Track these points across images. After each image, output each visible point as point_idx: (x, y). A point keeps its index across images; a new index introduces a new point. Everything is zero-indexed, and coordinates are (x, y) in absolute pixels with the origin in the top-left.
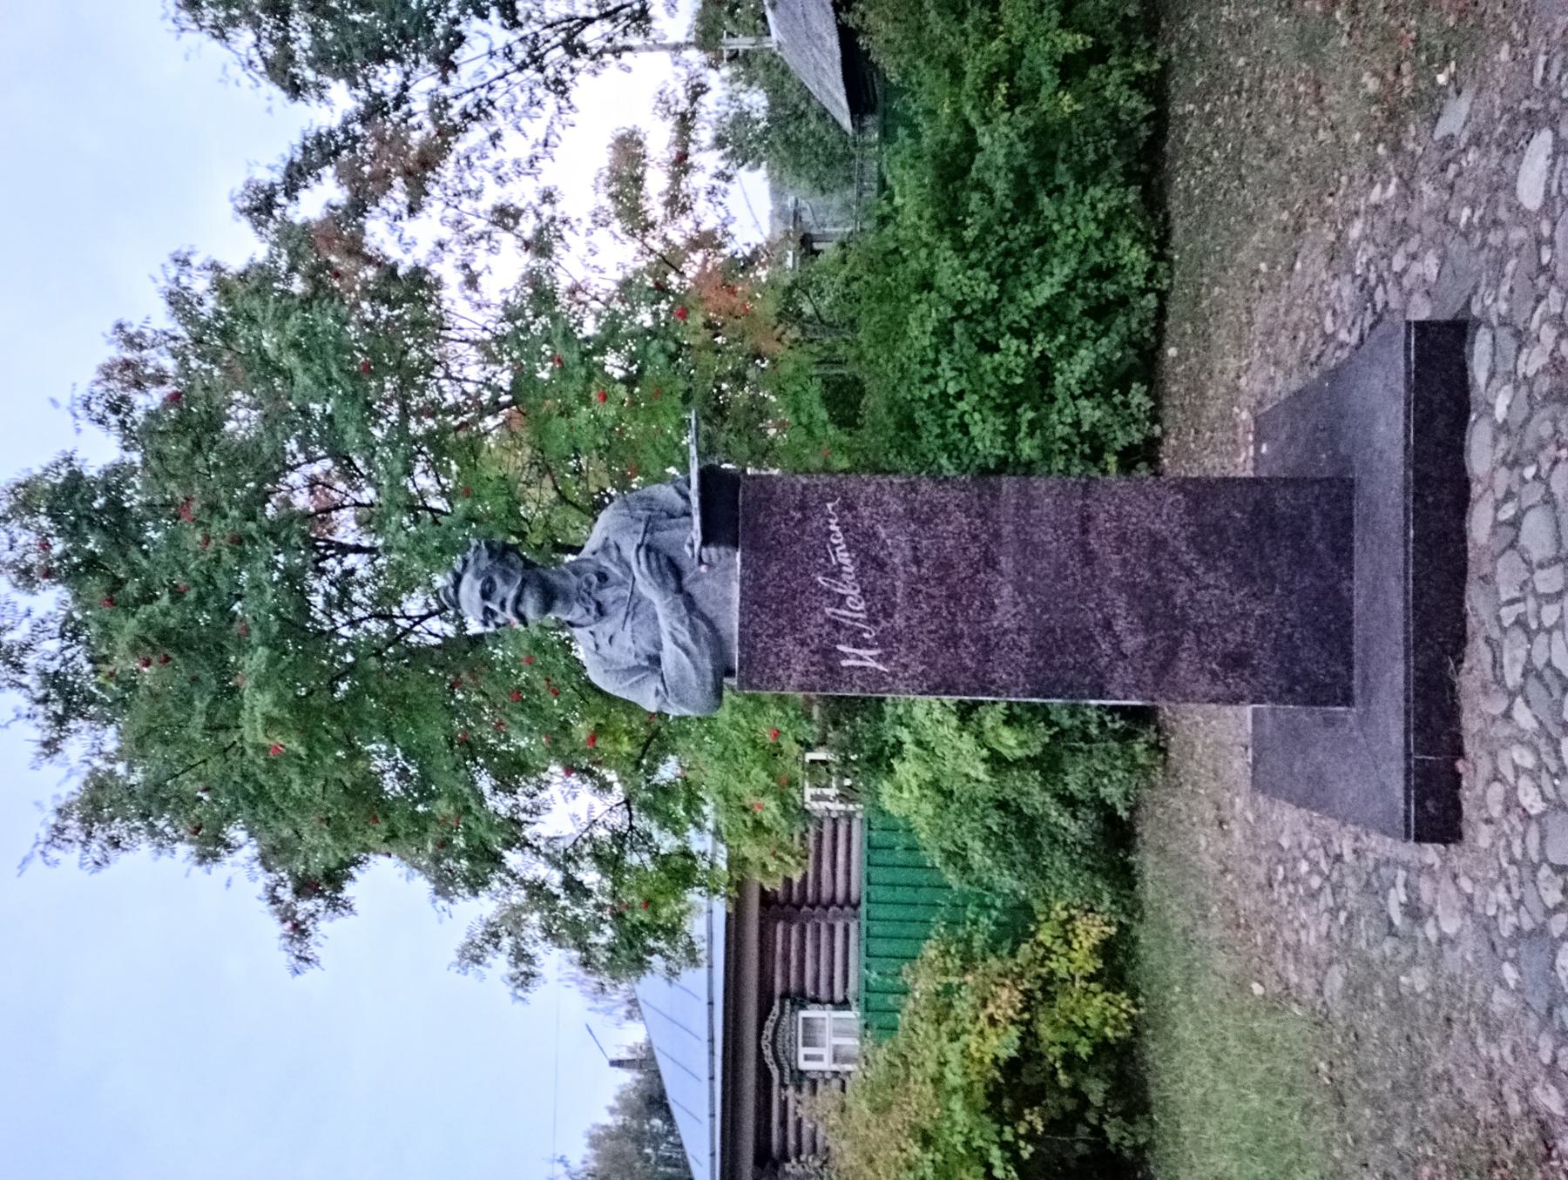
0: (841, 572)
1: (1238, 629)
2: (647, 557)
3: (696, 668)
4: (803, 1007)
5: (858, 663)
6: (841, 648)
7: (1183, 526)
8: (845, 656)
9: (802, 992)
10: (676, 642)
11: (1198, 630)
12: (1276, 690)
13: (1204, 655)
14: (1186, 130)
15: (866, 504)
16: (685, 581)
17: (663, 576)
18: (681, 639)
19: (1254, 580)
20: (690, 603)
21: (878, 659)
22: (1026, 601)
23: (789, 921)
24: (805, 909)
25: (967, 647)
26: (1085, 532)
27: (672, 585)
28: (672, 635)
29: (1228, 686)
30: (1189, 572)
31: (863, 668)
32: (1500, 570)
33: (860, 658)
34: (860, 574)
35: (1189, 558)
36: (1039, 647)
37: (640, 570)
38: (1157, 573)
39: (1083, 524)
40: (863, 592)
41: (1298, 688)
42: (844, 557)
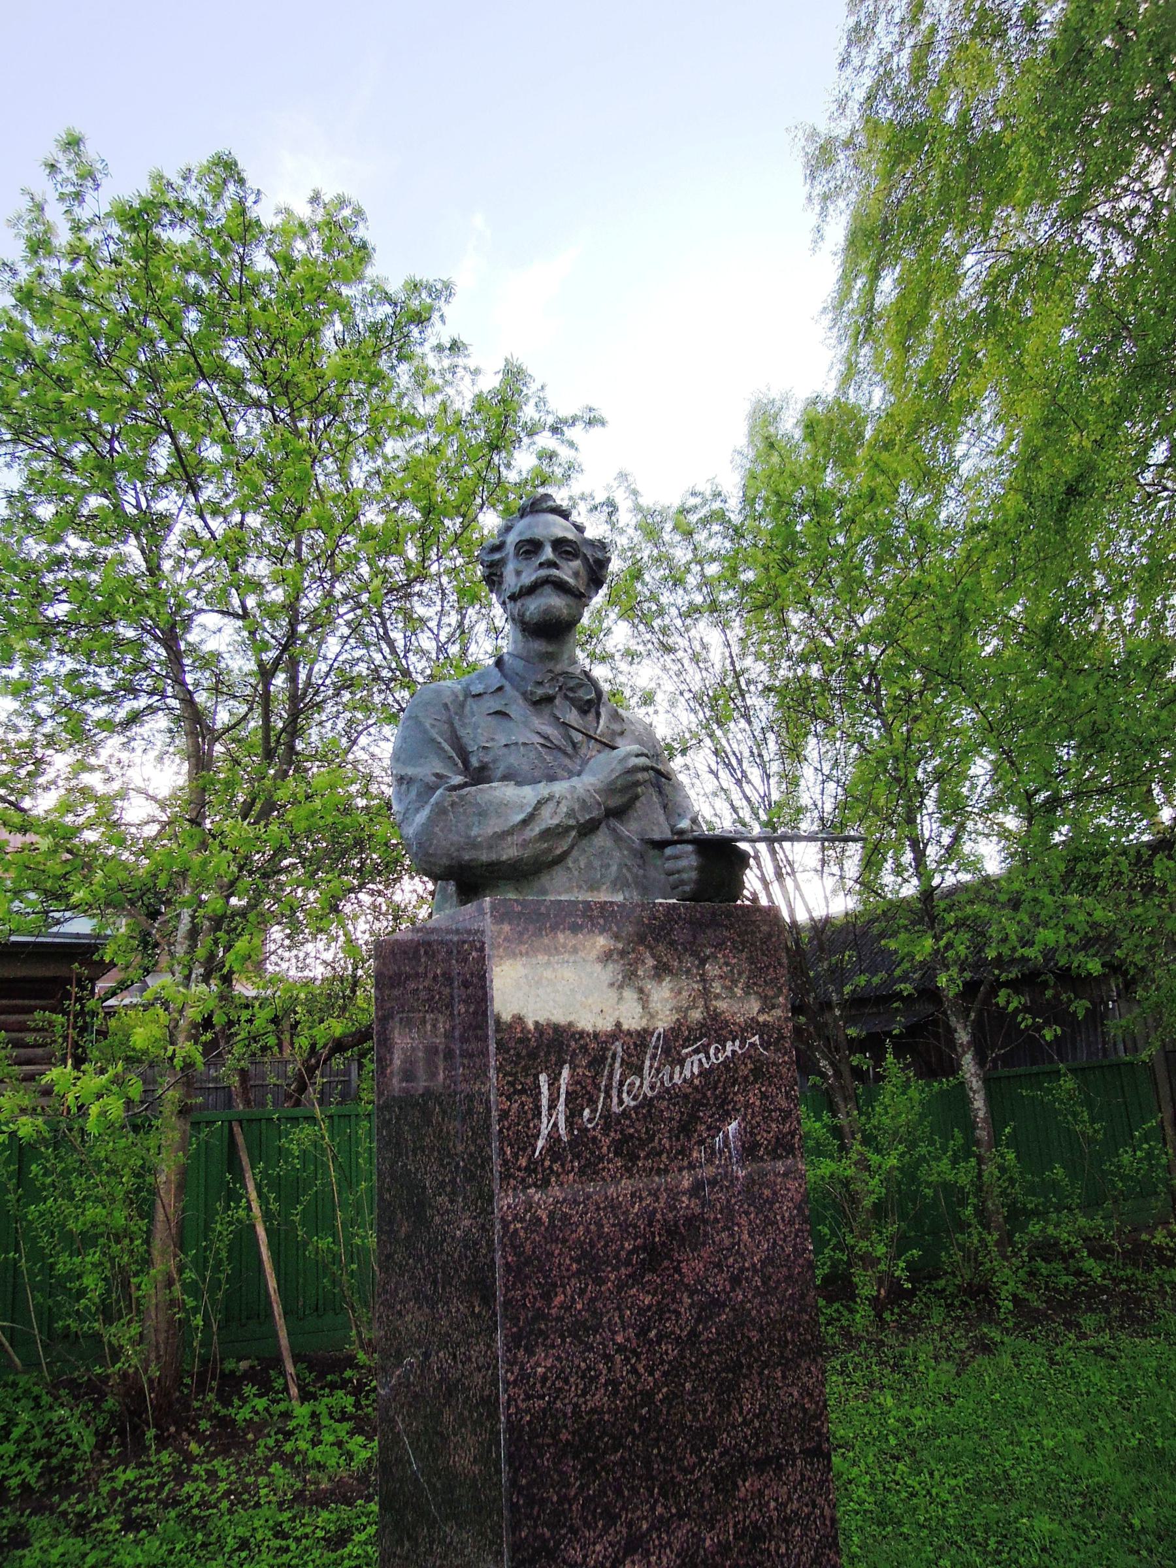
0: (672, 1064)
6: (566, 1072)
10: (540, 804)
14: (184, 1111)
15: (764, 1096)
18: (546, 812)
20: (588, 829)
21: (554, 1138)
22: (657, 1387)
25: (582, 1292)
28: (550, 798)
33: (552, 1107)
34: (668, 1094)
36: (590, 1426)
40: (648, 1102)
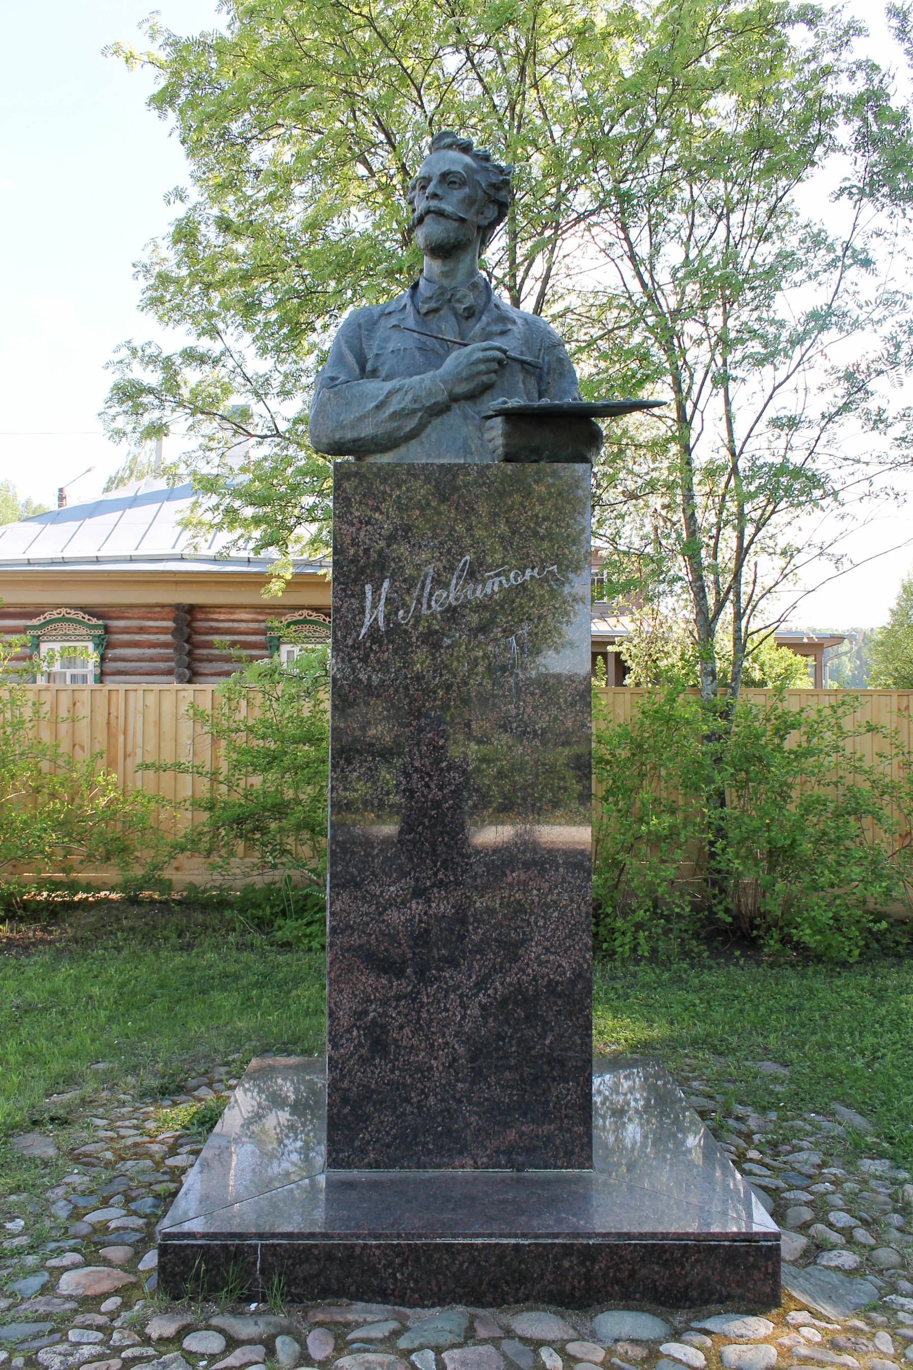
1: (414, 1042)
2: (494, 359)
3: (364, 417)
4: (97, 646)
5: (368, 604)
7: (534, 979)
8: (376, 590)
9: (109, 646)
10: (390, 394)
11: (413, 997)
12: (345, 1085)
13: (384, 1003)
16: (466, 405)
17: (470, 378)
18: (395, 399)
19: (473, 1059)
20: (438, 410)
21: (374, 627)
23: (176, 632)
24: (187, 646)
26: (527, 866)
27: (462, 388)
29: (349, 1031)
30: (480, 986)
31: (362, 611)
32: (480, 1349)
35: (497, 988)
37: (475, 350)
38: (479, 949)
39: (535, 863)
41: (347, 1110)
42: (493, 586)
